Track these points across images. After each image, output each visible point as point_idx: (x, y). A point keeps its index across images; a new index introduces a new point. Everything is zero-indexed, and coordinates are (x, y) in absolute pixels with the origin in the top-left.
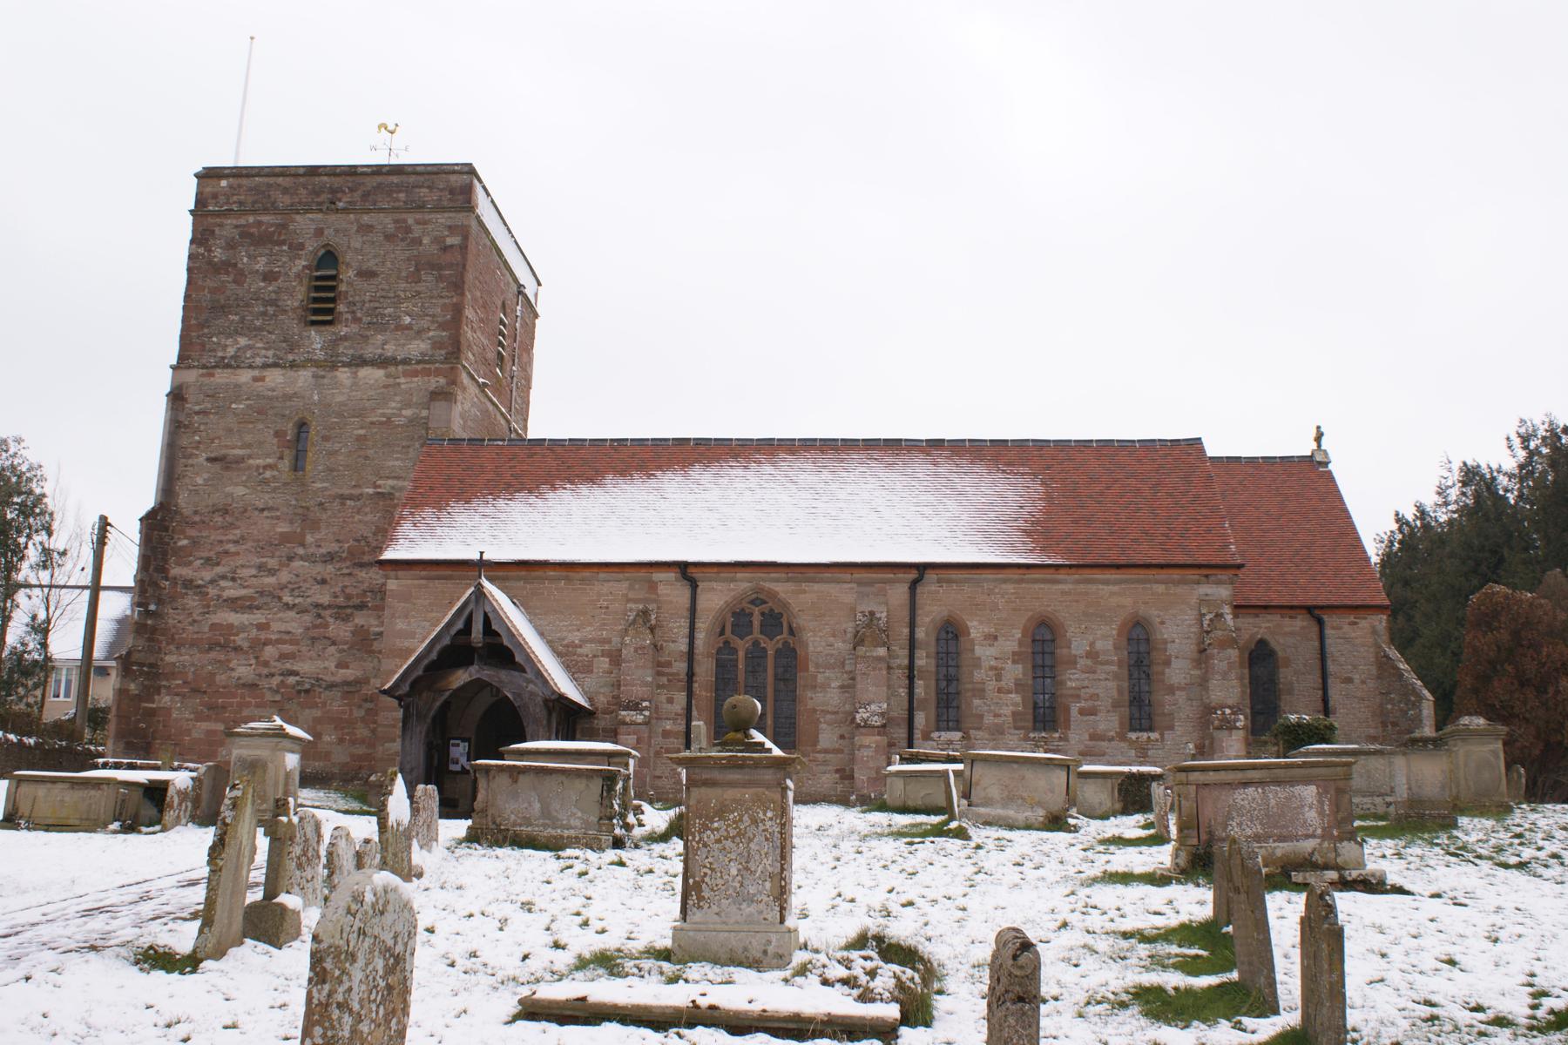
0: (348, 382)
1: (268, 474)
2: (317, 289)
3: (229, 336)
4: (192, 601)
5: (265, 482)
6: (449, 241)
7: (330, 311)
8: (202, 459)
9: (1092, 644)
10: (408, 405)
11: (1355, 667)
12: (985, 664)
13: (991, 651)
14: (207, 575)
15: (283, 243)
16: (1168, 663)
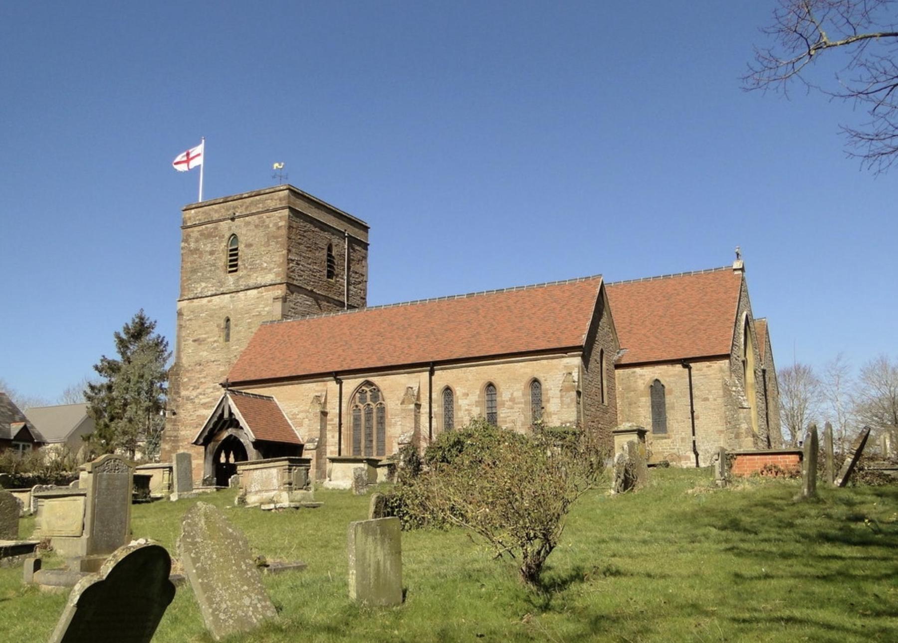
0: (243, 298)
1: (215, 345)
2: (231, 255)
3: (198, 283)
4: (189, 406)
5: (214, 349)
6: (280, 224)
7: (236, 265)
8: (190, 342)
9: (512, 394)
10: (267, 306)
11: (710, 391)
12: (464, 408)
13: (466, 402)
14: (194, 393)
15: (215, 236)
16: (548, 401)
